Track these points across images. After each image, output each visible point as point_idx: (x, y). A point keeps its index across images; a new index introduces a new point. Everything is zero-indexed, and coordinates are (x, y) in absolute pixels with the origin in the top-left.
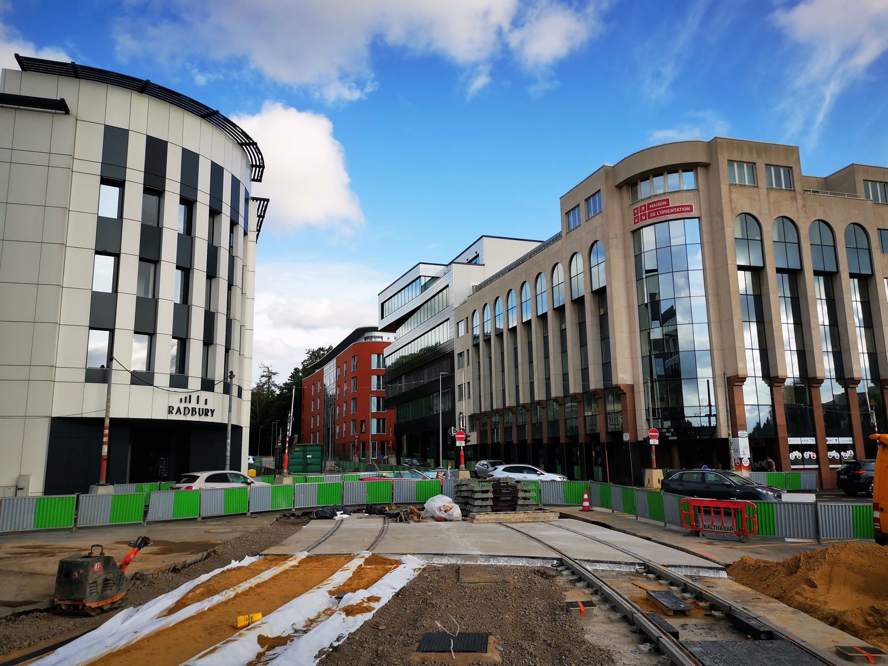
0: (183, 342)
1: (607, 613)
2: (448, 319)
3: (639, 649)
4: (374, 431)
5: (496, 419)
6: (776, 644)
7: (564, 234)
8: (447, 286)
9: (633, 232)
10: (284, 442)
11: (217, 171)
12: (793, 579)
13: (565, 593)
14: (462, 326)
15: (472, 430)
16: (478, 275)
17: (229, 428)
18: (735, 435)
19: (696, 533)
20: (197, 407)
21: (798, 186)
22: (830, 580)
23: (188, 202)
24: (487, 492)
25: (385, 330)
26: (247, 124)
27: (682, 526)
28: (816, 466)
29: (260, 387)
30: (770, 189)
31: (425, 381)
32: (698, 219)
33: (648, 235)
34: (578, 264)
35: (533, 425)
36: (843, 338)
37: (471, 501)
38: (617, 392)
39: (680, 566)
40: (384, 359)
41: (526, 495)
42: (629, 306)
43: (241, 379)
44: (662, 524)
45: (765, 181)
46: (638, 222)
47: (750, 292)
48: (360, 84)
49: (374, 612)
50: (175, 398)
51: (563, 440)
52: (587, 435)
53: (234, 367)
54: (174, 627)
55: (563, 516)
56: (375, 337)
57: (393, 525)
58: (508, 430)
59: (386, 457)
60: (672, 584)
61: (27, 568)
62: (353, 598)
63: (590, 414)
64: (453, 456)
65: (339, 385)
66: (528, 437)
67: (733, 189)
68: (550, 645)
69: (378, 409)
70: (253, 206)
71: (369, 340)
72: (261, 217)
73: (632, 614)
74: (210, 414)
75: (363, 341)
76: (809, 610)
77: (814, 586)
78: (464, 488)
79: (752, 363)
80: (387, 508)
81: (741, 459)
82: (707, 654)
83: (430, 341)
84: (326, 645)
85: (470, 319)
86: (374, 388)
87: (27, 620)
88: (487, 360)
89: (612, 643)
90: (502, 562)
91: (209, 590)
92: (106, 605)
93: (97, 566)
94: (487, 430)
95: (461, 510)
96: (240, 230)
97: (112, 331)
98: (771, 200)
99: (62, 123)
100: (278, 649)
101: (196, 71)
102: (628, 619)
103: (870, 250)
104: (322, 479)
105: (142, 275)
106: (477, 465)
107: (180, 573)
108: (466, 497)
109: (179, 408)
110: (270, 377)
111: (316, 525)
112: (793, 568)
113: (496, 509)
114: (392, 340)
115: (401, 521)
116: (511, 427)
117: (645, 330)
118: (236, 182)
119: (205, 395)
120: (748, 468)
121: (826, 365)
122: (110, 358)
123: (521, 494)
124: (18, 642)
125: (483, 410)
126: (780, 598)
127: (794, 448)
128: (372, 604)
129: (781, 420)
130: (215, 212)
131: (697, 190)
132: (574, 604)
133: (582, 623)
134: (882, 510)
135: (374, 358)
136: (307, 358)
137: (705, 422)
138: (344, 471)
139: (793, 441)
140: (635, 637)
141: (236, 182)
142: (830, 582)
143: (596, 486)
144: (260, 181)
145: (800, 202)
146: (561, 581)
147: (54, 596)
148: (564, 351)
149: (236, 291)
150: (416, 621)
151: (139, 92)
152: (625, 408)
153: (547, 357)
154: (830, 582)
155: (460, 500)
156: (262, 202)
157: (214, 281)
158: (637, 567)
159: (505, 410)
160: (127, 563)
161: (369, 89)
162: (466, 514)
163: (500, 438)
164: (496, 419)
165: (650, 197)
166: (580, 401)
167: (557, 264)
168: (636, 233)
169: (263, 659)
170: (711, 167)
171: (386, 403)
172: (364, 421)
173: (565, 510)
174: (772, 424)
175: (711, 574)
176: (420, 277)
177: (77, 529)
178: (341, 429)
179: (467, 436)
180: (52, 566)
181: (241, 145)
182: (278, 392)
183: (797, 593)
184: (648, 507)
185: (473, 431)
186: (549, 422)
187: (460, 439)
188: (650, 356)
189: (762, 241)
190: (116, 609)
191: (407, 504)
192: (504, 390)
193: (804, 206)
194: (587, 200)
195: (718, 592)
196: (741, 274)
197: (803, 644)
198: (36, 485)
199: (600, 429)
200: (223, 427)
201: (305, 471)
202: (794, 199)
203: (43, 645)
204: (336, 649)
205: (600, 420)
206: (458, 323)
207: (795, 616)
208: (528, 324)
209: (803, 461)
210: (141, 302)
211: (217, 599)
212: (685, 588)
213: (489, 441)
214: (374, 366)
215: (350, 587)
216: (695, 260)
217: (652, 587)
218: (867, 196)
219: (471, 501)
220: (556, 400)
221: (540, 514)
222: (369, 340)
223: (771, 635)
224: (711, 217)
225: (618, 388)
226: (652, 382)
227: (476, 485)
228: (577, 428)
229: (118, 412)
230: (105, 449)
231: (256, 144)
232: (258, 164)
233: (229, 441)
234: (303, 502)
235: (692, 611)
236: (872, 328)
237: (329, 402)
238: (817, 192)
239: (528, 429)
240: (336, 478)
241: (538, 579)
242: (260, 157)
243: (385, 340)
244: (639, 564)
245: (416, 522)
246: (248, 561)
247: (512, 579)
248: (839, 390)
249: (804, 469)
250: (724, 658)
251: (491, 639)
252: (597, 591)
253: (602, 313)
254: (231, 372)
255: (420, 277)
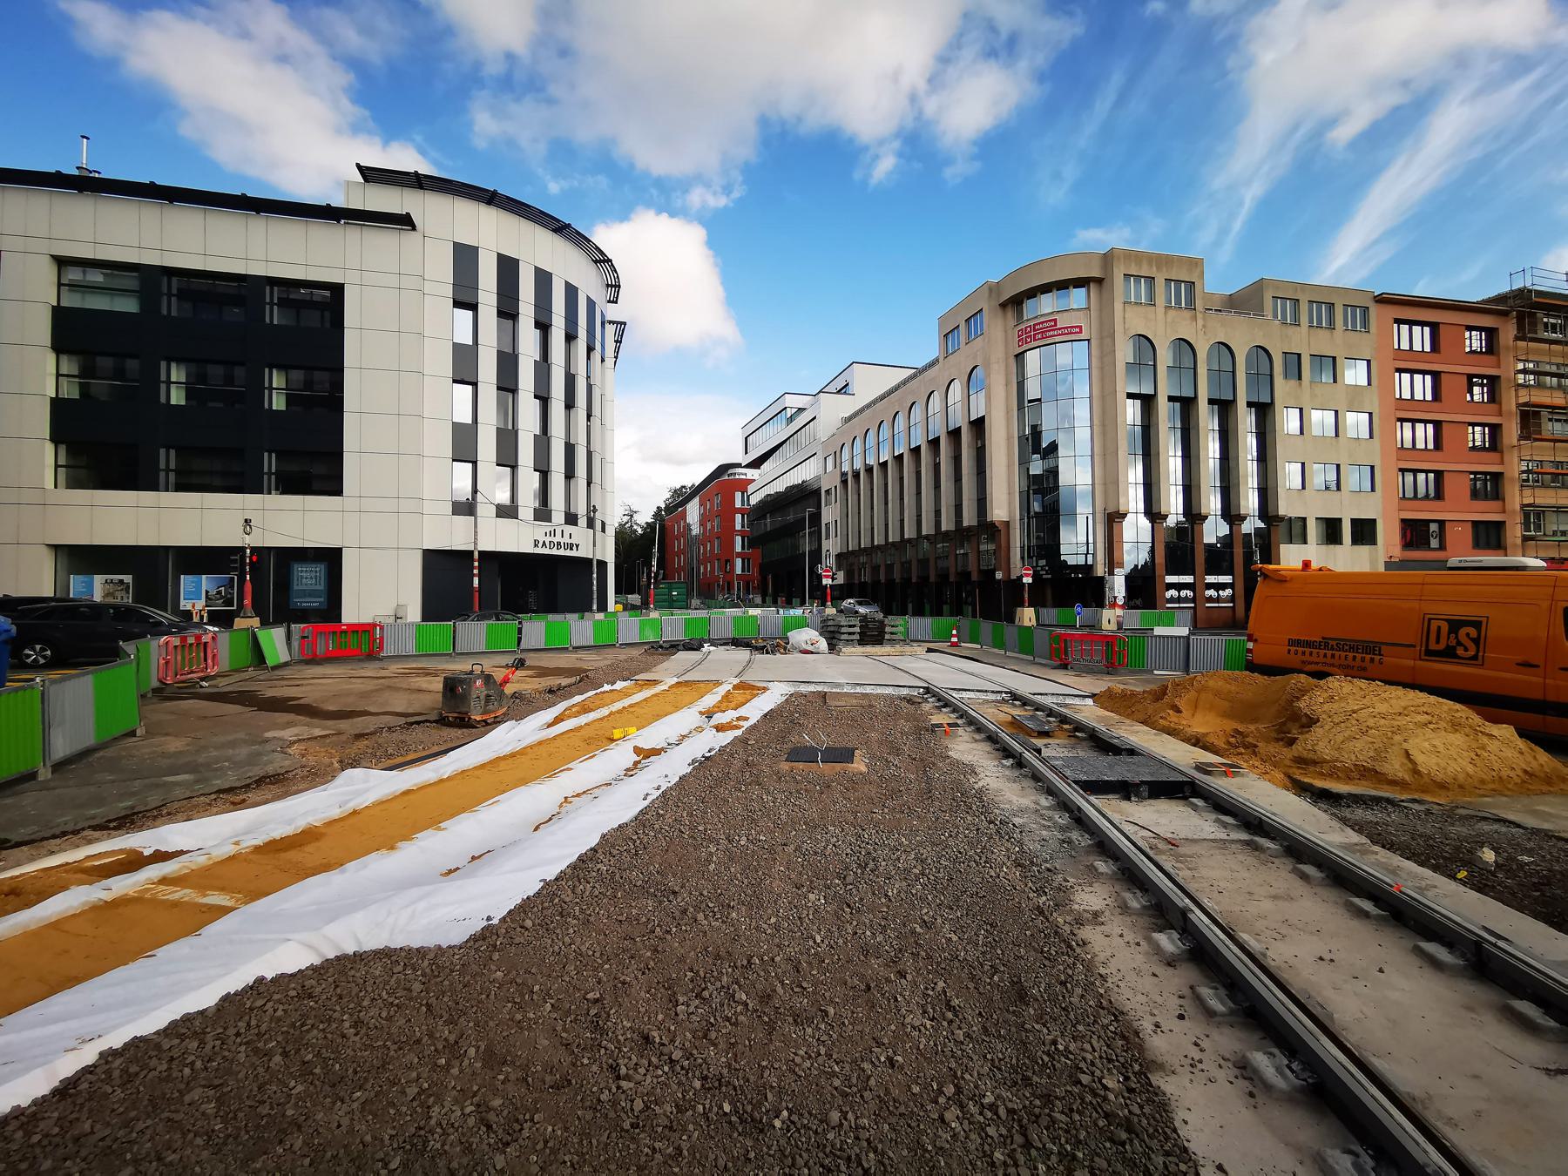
0: (545, 474)
1: (971, 734)
2: (815, 454)
3: (1002, 764)
4: (739, 571)
5: (863, 559)
6: (1136, 759)
7: (941, 360)
8: (815, 418)
9: (1016, 356)
10: (649, 577)
11: (571, 292)
12: (1159, 704)
13: (931, 717)
14: (830, 461)
15: (839, 569)
16: (847, 405)
17: (595, 563)
18: (1111, 573)
19: (1064, 666)
20: (562, 541)
21: (1199, 304)
22: (1195, 706)
23: (543, 326)
24: (854, 626)
25: (749, 466)
26: (606, 237)
27: (1051, 659)
28: (1192, 605)
29: (622, 525)
30: (1168, 308)
31: (790, 518)
32: (1087, 342)
33: (1032, 358)
34: (957, 391)
35: (902, 564)
36: (1233, 473)
37: (837, 636)
38: (990, 530)
39: (1046, 694)
40: (748, 497)
41: (894, 630)
42: (1009, 438)
43: (604, 514)
44: (1031, 658)
45: (1163, 297)
46: (1031, 341)
47: (1138, 422)
48: (727, 189)
49: (744, 729)
50: (540, 531)
51: (932, 579)
52: (957, 574)
53: (595, 501)
54: (554, 738)
55: (930, 650)
56: (739, 474)
57: (759, 657)
58: (876, 569)
59: (751, 596)
60: (1037, 710)
61: (416, 686)
62: (721, 718)
63: (962, 551)
64: (820, 595)
65: (702, 523)
66: (897, 576)
67: (1126, 307)
68: (915, 759)
69: (743, 548)
70: (610, 329)
71: (732, 477)
72: (618, 342)
73: (997, 733)
74: (575, 548)
75: (727, 478)
76: (1172, 732)
77: (1179, 711)
78: (830, 623)
79: (1134, 499)
80: (753, 642)
81: (1115, 598)
82: (1068, 767)
83: (795, 478)
84: (699, 756)
85: (838, 454)
86: (738, 527)
87: (418, 729)
88: (856, 497)
89: (975, 759)
90: (868, 690)
91: (585, 709)
92: (490, 717)
93: (479, 683)
94: (854, 570)
95: (828, 644)
96: (597, 355)
97: (475, 463)
98: (1169, 320)
99: (409, 238)
100: (652, 759)
101: (549, 177)
102: (992, 739)
103: (1271, 376)
104: (689, 614)
105: (501, 405)
106: (844, 604)
107: (555, 694)
108: (833, 632)
109: (544, 542)
110: (632, 516)
111: (682, 656)
112: (1160, 694)
113: (862, 642)
114: (756, 477)
115: (768, 653)
116: (880, 566)
117: (1024, 462)
118: (591, 304)
119: (569, 529)
120: (1122, 607)
121: (1212, 503)
122: (475, 491)
123: (888, 629)
124: (414, 746)
125: (850, 549)
126: (1144, 723)
127: (1171, 586)
128: (741, 723)
129: (1160, 559)
130: (570, 337)
131: (1088, 308)
132: (941, 725)
133: (947, 742)
134: (1256, 641)
135: (738, 495)
136: (669, 497)
137: (1081, 561)
138: (709, 607)
139: (1170, 579)
140: (1000, 754)
141: (591, 304)
142: (1196, 707)
143: (966, 622)
144: (616, 302)
145: (1200, 322)
146: (926, 707)
147: (441, 709)
148: (937, 486)
149: (595, 421)
150: (783, 738)
151: (486, 203)
152: (999, 547)
153: (919, 493)
154: (1196, 707)
155: (828, 635)
156: (619, 326)
157: (573, 412)
158: (1004, 695)
159: (874, 549)
160: (506, 680)
161: (736, 194)
162: (832, 648)
163: (866, 577)
164: (863, 559)
165: (1036, 317)
166: (951, 539)
167: (933, 392)
168: (1020, 357)
169: (639, 766)
170: (1105, 284)
171: (752, 541)
172: (728, 561)
173: (932, 645)
174: (1149, 567)
175: (1077, 701)
176: (786, 408)
177: (455, 654)
178: (706, 568)
179: (834, 574)
180: (437, 685)
181: (596, 262)
182: (640, 531)
183: (1161, 718)
184: (1017, 642)
185: (840, 570)
186: (919, 561)
187: (827, 577)
188: (1028, 491)
189: (1155, 366)
190: (499, 722)
191: (772, 638)
192: (873, 528)
193: (1204, 326)
194: (967, 321)
195: (1083, 717)
196: (1130, 402)
197: (1163, 759)
198: (414, 613)
199: (972, 567)
200: (588, 562)
201: (671, 607)
202: (1195, 318)
203: (436, 749)
204: (707, 759)
205: (972, 558)
206: (825, 458)
207: (1158, 738)
208: (899, 458)
209: (1179, 600)
210: (501, 433)
211: (592, 716)
212: (1051, 713)
213: (856, 582)
214: (738, 504)
215: (719, 708)
216: (1082, 390)
217: (1017, 712)
218: (1275, 316)
219: (837, 636)
220: (927, 537)
221: (907, 648)
222: (732, 477)
223: (1132, 752)
224: (1101, 338)
225: (993, 524)
226: (1029, 518)
227: (843, 621)
228: (948, 568)
229: (486, 545)
230: (476, 581)
231: (611, 261)
232: (614, 283)
233: (595, 576)
234: (670, 635)
235: (1056, 733)
236: (1266, 460)
237: (693, 542)
238: (1220, 311)
239: (897, 568)
240: (703, 614)
241: (904, 704)
242: (616, 275)
243: (749, 477)
244: (1006, 693)
245: (782, 654)
246: (619, 685)
247: (879, 705)
248: (1224, 529)
249: (1179, 608)
250: (1085, 769)
251: (857, 752)
252: (963, 715)
253: (979, 445)
254: (594, 506)
255: (786, 408)
